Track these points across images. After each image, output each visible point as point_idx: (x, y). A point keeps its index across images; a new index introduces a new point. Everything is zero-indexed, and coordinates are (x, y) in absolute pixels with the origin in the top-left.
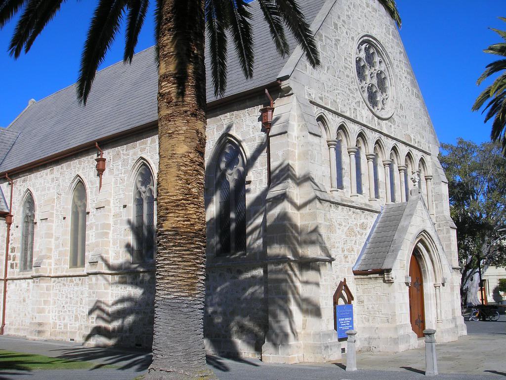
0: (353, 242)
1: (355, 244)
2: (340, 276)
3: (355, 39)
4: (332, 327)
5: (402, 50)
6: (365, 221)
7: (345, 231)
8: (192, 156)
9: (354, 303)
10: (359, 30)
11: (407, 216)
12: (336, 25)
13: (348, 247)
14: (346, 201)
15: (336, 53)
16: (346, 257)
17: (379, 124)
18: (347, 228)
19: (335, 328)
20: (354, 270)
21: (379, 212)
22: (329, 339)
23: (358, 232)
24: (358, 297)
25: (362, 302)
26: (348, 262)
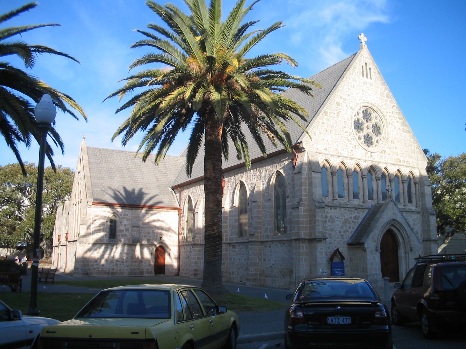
5: (395, 105)
8: (215, 208)
14: (342, 205)
23: (352, 221)
25: (352, 260)
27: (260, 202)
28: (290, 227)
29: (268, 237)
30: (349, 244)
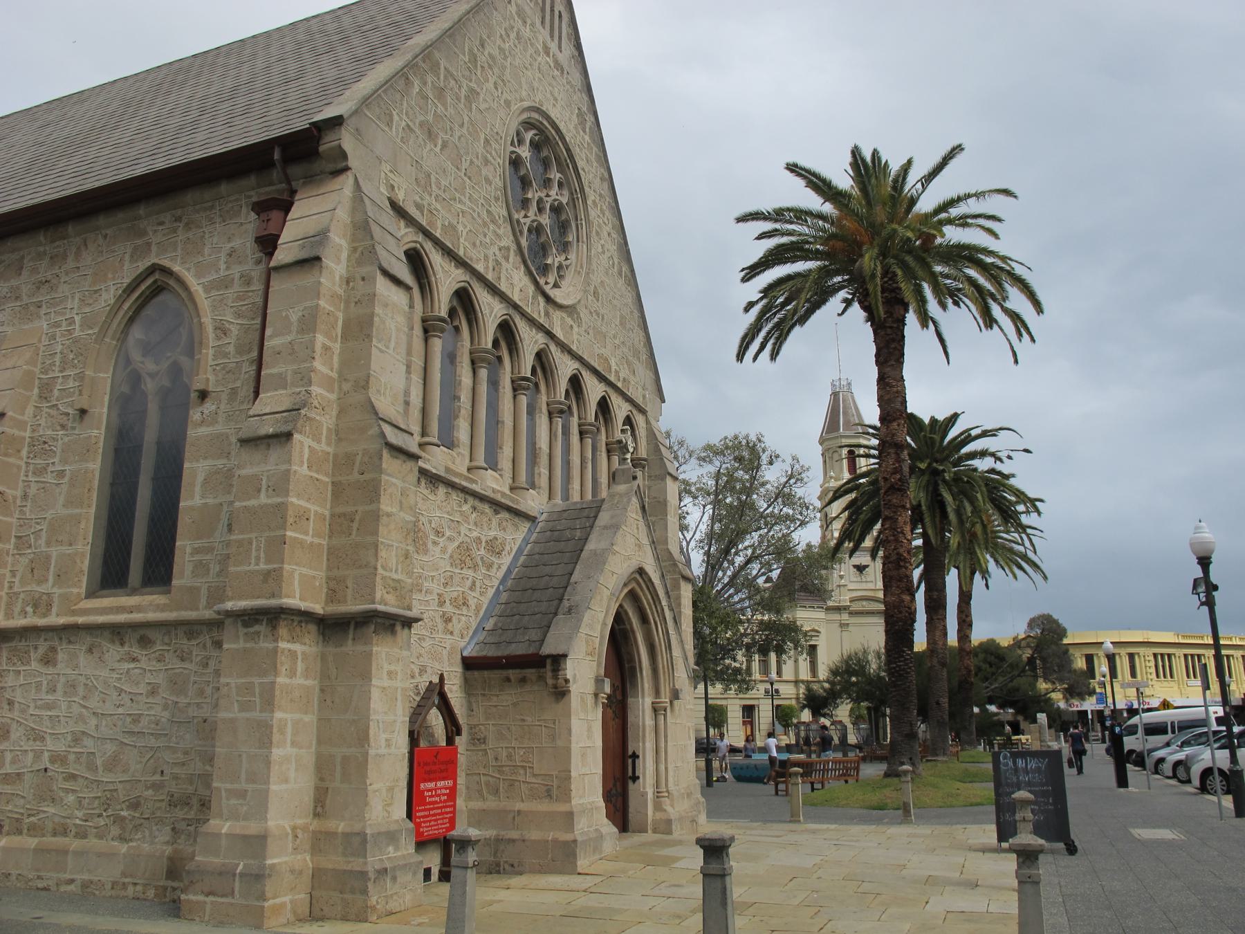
0: (469, 583)
1: (471, 589)
2: (429, 670)
3: (514, 108)
4: (400, 810)
6: (500, 534)
7: (450, 551)
9: (461, 742)
10: (524, 94)
11: (605, 527)
12: (474, 59)
13: (455, 594)
15: (466, 119)
16: (448, 620)
17: (547, 314)
18: (456, 544)
19: (410, 815)
20: (465, 654)
21: (532, 519)
22: (391, 849)
24: (471, 727)
25: (483, 741)
26: (452, 633)
27: (21, 425)
28: (196, 551)
29: (41, 604)
30: (469, 664)
